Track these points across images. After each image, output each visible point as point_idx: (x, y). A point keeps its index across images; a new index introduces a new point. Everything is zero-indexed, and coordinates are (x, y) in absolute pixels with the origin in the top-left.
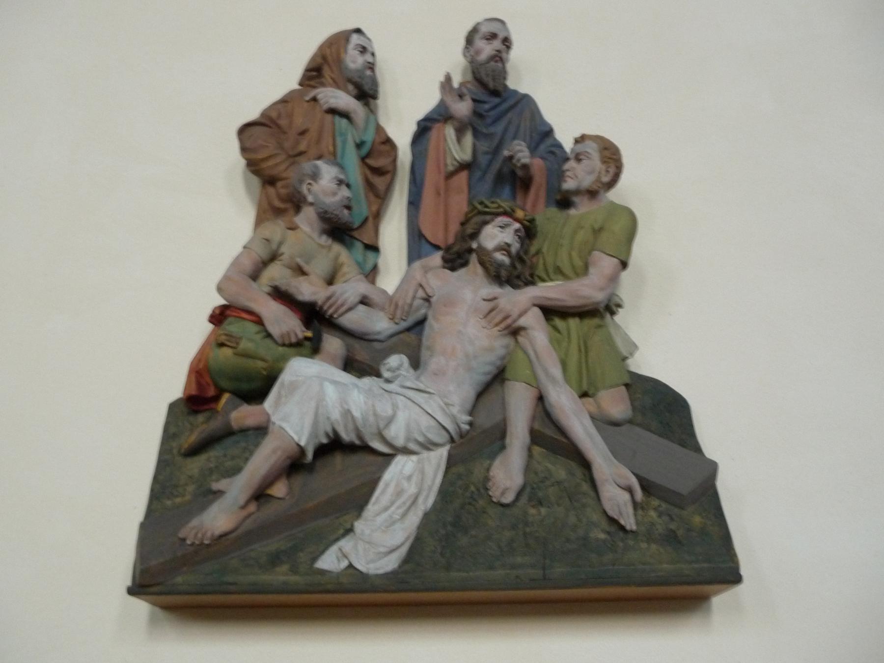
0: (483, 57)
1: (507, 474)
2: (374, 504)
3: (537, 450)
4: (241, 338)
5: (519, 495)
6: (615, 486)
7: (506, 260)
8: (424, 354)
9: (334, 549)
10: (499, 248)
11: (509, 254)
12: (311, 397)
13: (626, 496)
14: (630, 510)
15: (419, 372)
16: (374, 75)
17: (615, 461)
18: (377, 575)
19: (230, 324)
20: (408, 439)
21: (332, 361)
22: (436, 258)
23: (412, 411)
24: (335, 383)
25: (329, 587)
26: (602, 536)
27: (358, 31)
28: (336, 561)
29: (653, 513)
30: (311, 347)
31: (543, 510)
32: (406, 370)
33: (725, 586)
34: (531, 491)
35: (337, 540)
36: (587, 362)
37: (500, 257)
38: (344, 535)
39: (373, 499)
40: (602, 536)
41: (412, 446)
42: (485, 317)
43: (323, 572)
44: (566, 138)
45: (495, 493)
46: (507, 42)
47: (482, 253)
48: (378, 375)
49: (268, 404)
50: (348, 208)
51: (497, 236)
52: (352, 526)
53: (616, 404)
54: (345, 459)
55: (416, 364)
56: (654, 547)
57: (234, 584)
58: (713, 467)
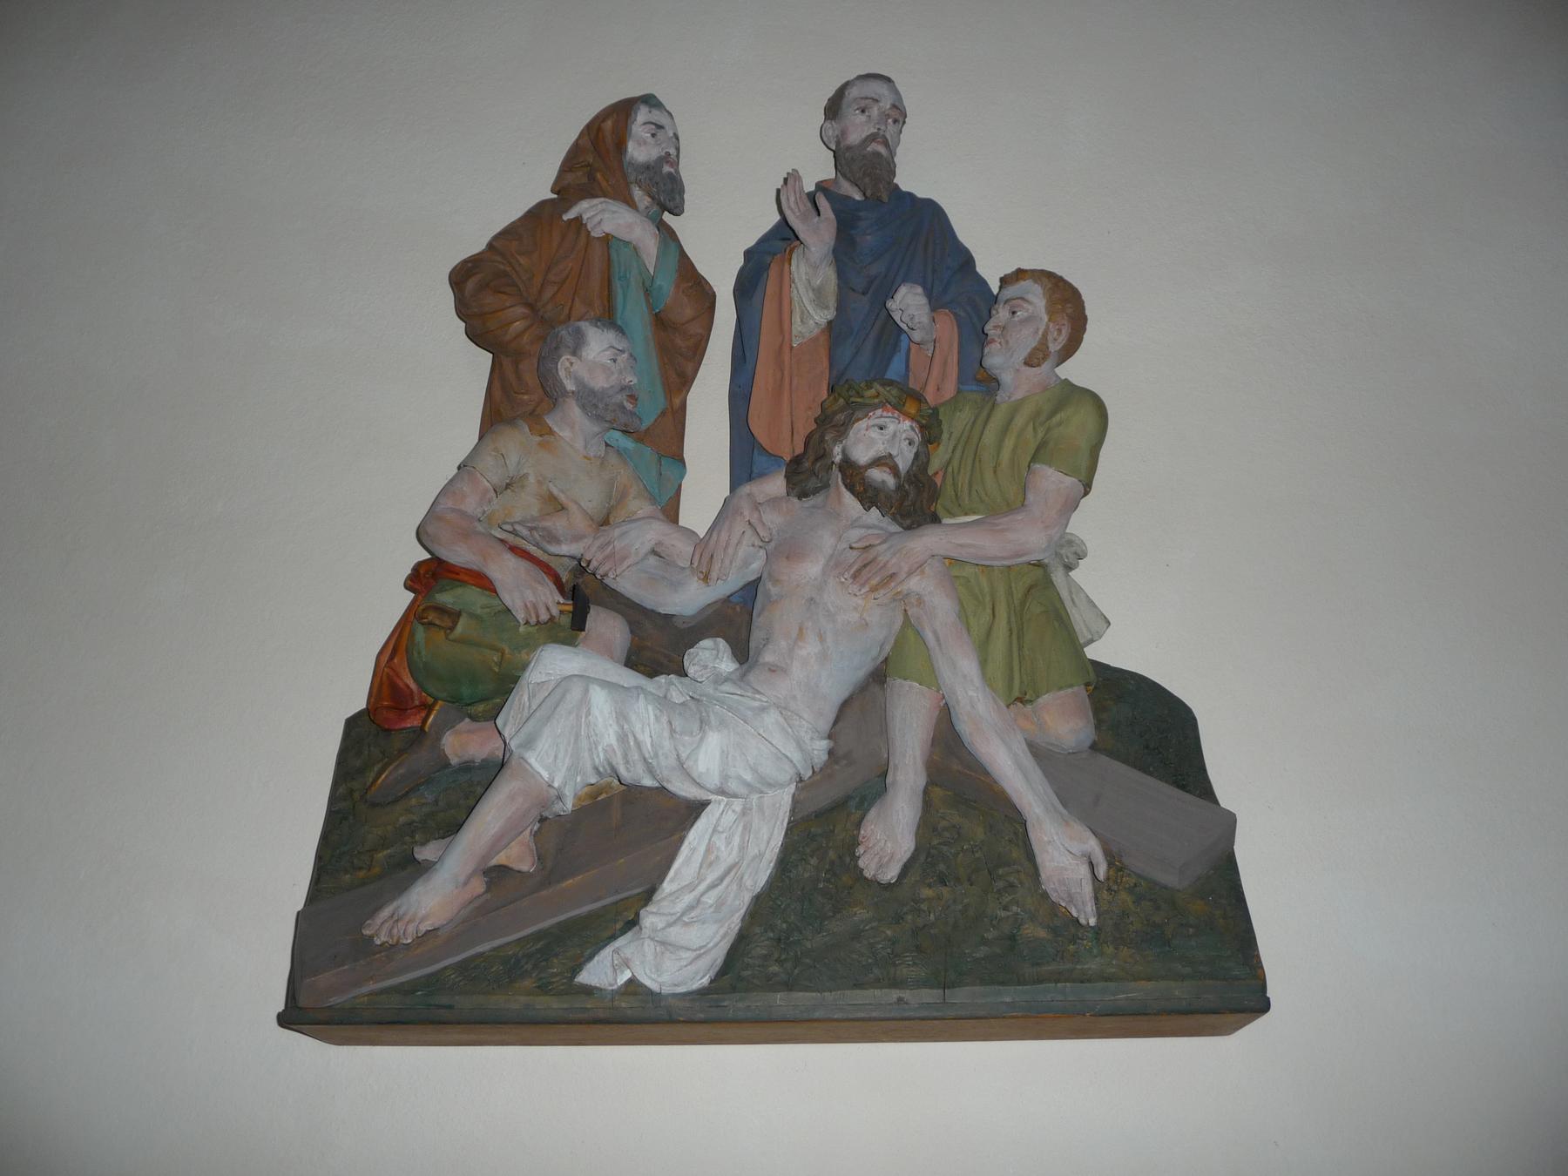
0: (854, 138)
1: (889, 839)
2: (672, 881)
3: (937, 792)
4: (459, 614)
5: (906, 869)
6: (1066, 857)
7: (891, 481)
8: (757, 636)
9: (607, 952)
10: (877, 462)
11: (894, 470)
12: (576, 723)
13: (1084, 870)
14: (1088, 889)
15: (745, 666)
16: (677, 172)
17: (1064, 811)
18: (675, 995)
19: (441, 591)
20: (725, 777)
21: (607, 651)
22: (776, 484)
23: (737, 763)
24: (605, 684)
25: (601, 1014)
26: (1042, 933)
27: (650, 101)
28: (610, 971)
29: (1124, 896)
30: (571, 626)
31: (945, 891)
32: (727, 665)
33: (1231, 1018)
34: (928, 857)
35: (613, 938)
36: (1020, 648)
37: (879, 475)
38: (623, 932)
39: (672, 873)
40: (1042, 933)
41: (733, 786)
42: (855, 577)
43: (588, 991)
44: (991, 270)
45: (868, 865)
46: (898, 114)
47: (853, 475)
48: (682, 673)
49: (508, 720)
50: (633, 398)
51: (880, 438)
52: (637, 915)
53: (1066, 721)
54: (636, 825)
55: (742, 653)
56: (1125, 951)
57: (450, 1007)
58: (1230, 821)
